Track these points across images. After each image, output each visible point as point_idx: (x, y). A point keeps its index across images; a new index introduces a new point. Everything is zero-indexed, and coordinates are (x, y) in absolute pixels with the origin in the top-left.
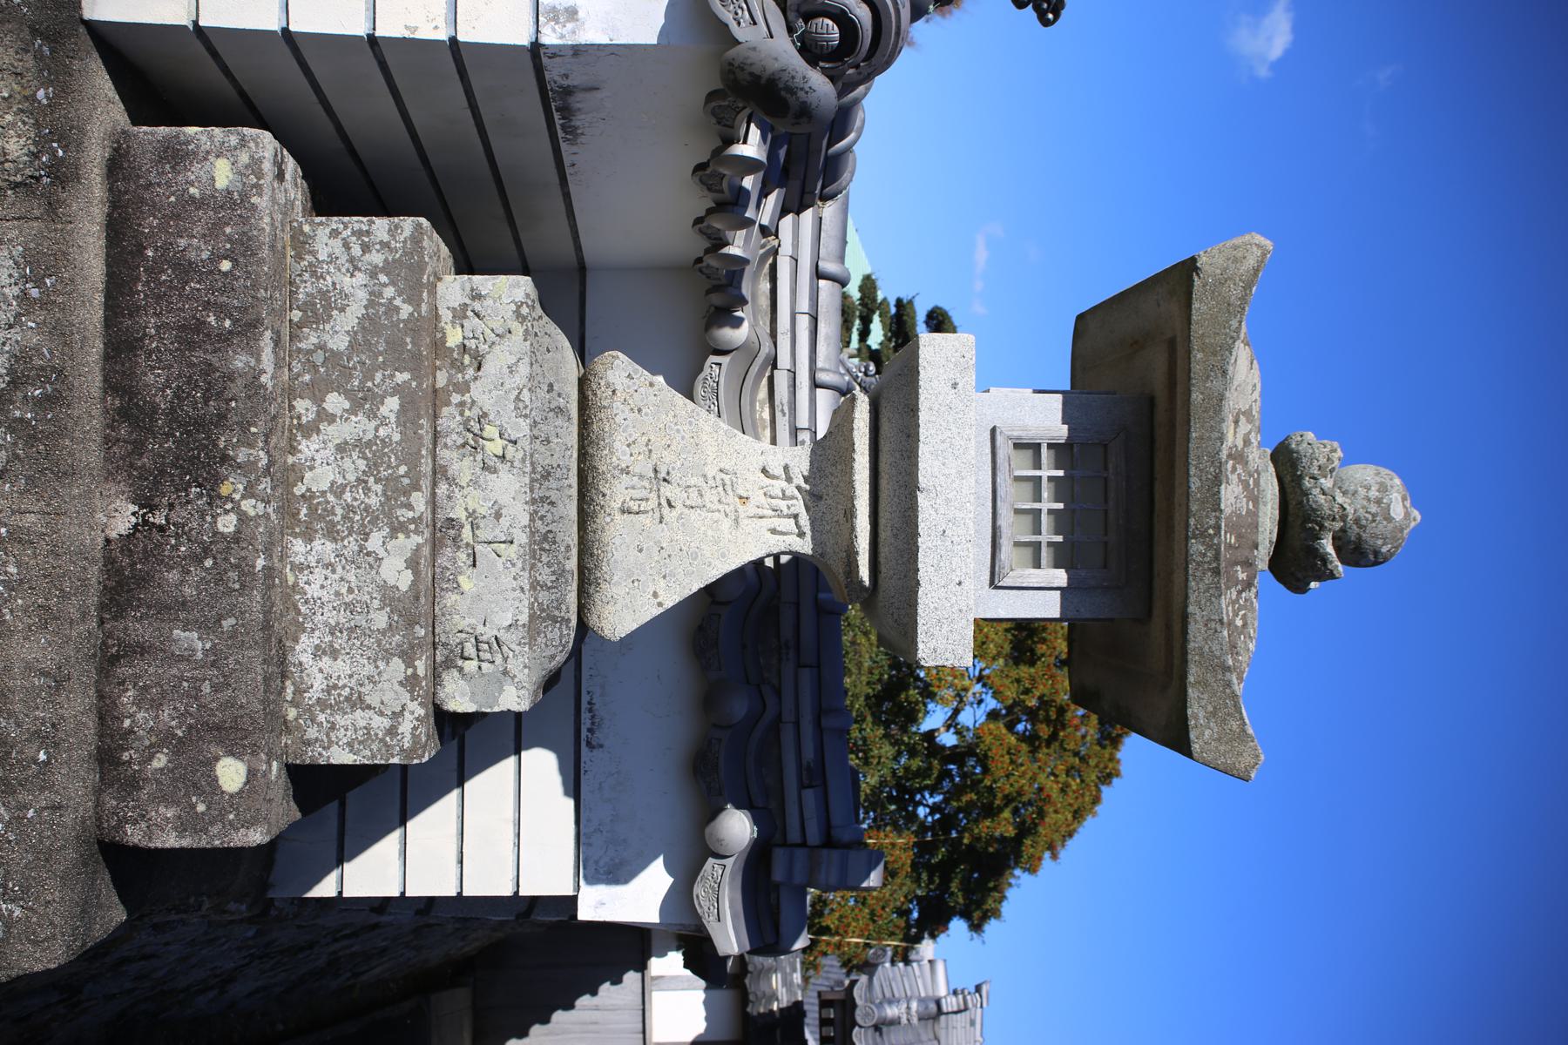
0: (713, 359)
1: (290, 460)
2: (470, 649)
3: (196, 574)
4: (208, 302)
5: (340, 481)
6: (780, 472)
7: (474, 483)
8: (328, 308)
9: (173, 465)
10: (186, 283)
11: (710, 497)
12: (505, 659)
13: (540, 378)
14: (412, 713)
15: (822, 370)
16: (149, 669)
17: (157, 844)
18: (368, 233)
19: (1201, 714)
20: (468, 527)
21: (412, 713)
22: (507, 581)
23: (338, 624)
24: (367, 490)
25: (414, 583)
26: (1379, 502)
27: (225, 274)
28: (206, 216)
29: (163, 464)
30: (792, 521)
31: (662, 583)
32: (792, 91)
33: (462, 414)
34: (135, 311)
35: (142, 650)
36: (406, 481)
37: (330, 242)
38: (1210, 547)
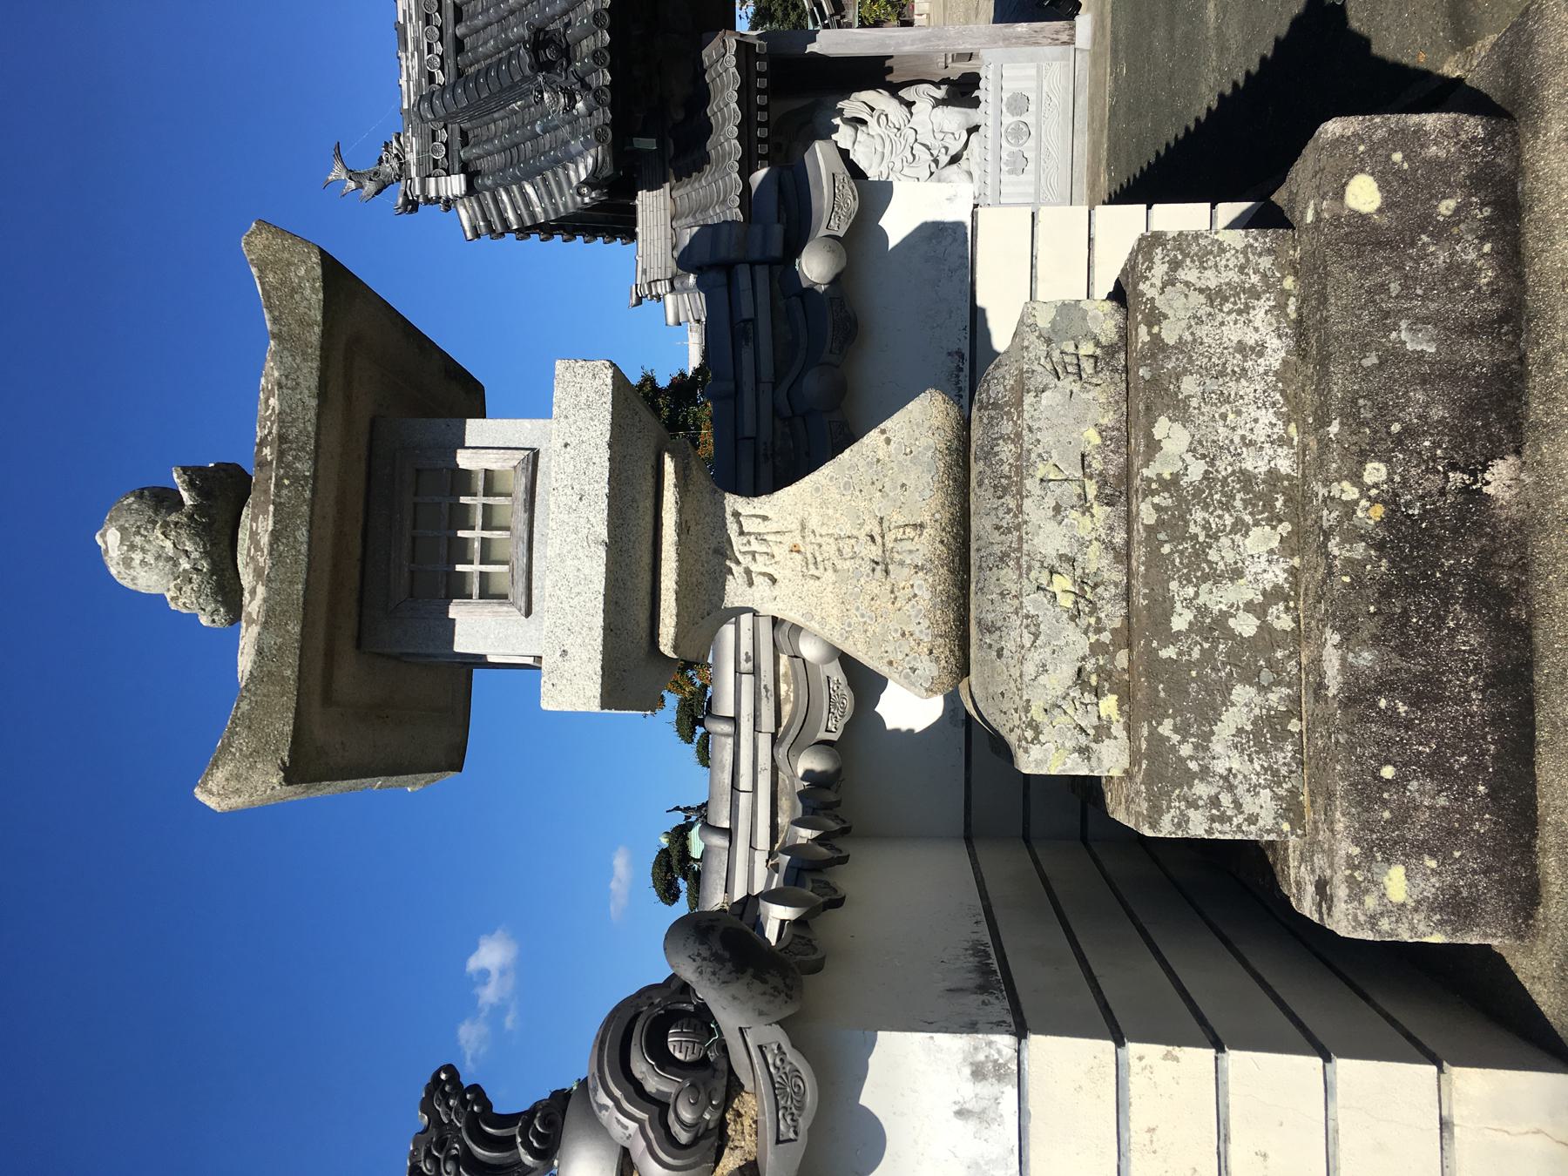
0: (834, 737)
1: (1296, 561)
2: (1088, 366)
3: (1411, 415)
4: (1407, 729)
5: (1238, 537)
6: (757, 580)
7: (1083, 544)
8: (1257, 734)
9: (1443, 539)
10: (1435, 752)
11: (830, 549)
12: (1048, 356)
13: (1012, 662)
14: (1152, 285)
15: (727, 735)
16: (1464, 308)
17: (1446, 117)
18: (1213, 819)
19: (307, 292)
20: (1090, 497)
21: (1152, 285)
22: (1047, 438)
23: (1238, 380)
24: (1206, 526)
25: (1152, 424)
26: (132, 547)
27: (1388, 762)
28: (1414, 832)
29: (1454, 540)
30: (746, 529)
31: (880, 455)
32: (716, 957)
33: (1099, 620)
34: (1496, 720)
35: (1470, 329)
36: (1162, 536)
37: (1257, 810)
38: (289, 466)
